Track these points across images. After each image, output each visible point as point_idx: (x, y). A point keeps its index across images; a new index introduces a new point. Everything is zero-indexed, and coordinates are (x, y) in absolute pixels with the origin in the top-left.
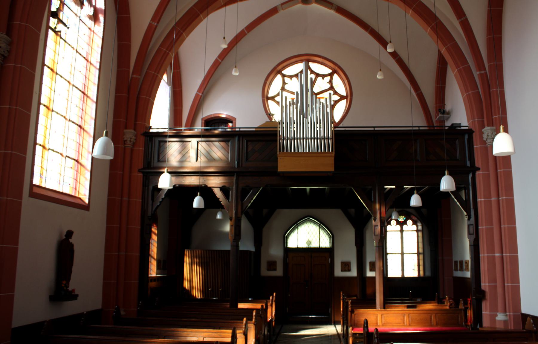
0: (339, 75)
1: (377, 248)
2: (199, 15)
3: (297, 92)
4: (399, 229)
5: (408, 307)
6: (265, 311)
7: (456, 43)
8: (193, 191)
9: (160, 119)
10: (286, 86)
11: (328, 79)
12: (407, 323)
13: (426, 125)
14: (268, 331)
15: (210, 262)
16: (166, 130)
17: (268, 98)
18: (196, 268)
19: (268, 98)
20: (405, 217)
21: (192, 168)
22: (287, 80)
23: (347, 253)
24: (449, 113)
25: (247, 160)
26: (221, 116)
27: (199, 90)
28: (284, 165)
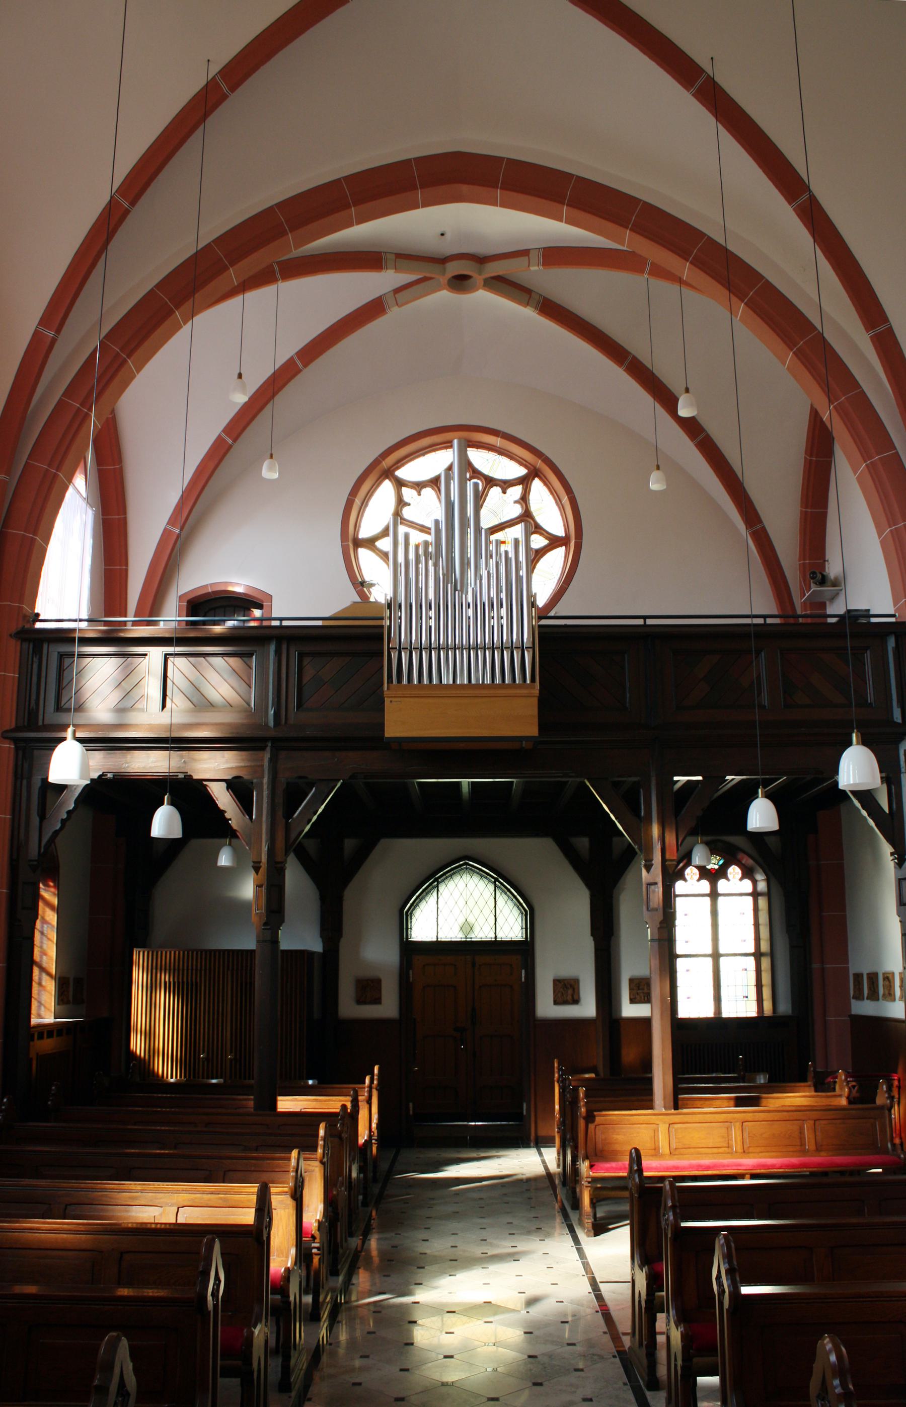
0: (546, 483)
1: (656, 944)
2: (171, 313)
3: (437, 522)
5: (739, 1102)
6: (352, 1117)
7: (863, 393)
8: (149, 791)
9: (63, 590)
10: (410, 506)
11: (516, 492)
12: (736, 1145)
13: (775, 612)
14: (361, 1170)
15: (204, 980)
16: (84, 625)
17: (358, 543)
18: (161, 997)
19: (358, 543)
20: (722, 857)
21: (151, 727)
22: (408, 494)
23: (569, 955)
24: (835, 583)
25: (300, 705)
26: (231, 589)
27: (172, 521)
28: (402, 720)
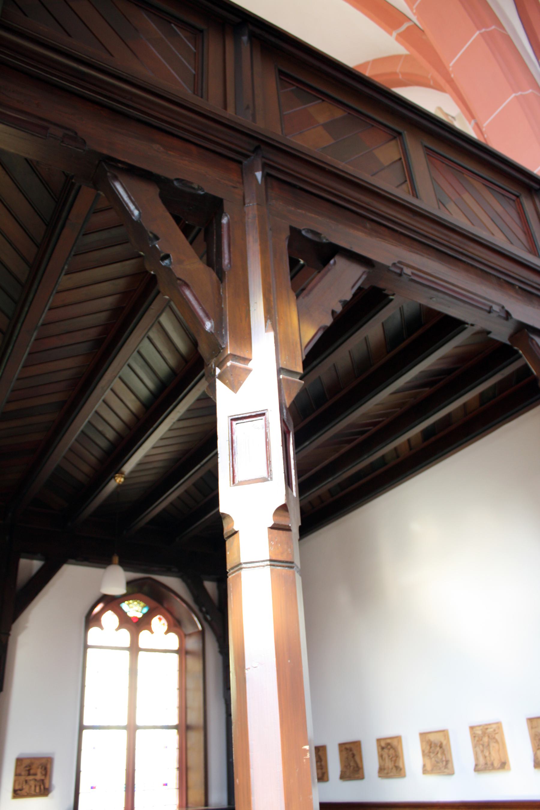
4: (127, 643)
